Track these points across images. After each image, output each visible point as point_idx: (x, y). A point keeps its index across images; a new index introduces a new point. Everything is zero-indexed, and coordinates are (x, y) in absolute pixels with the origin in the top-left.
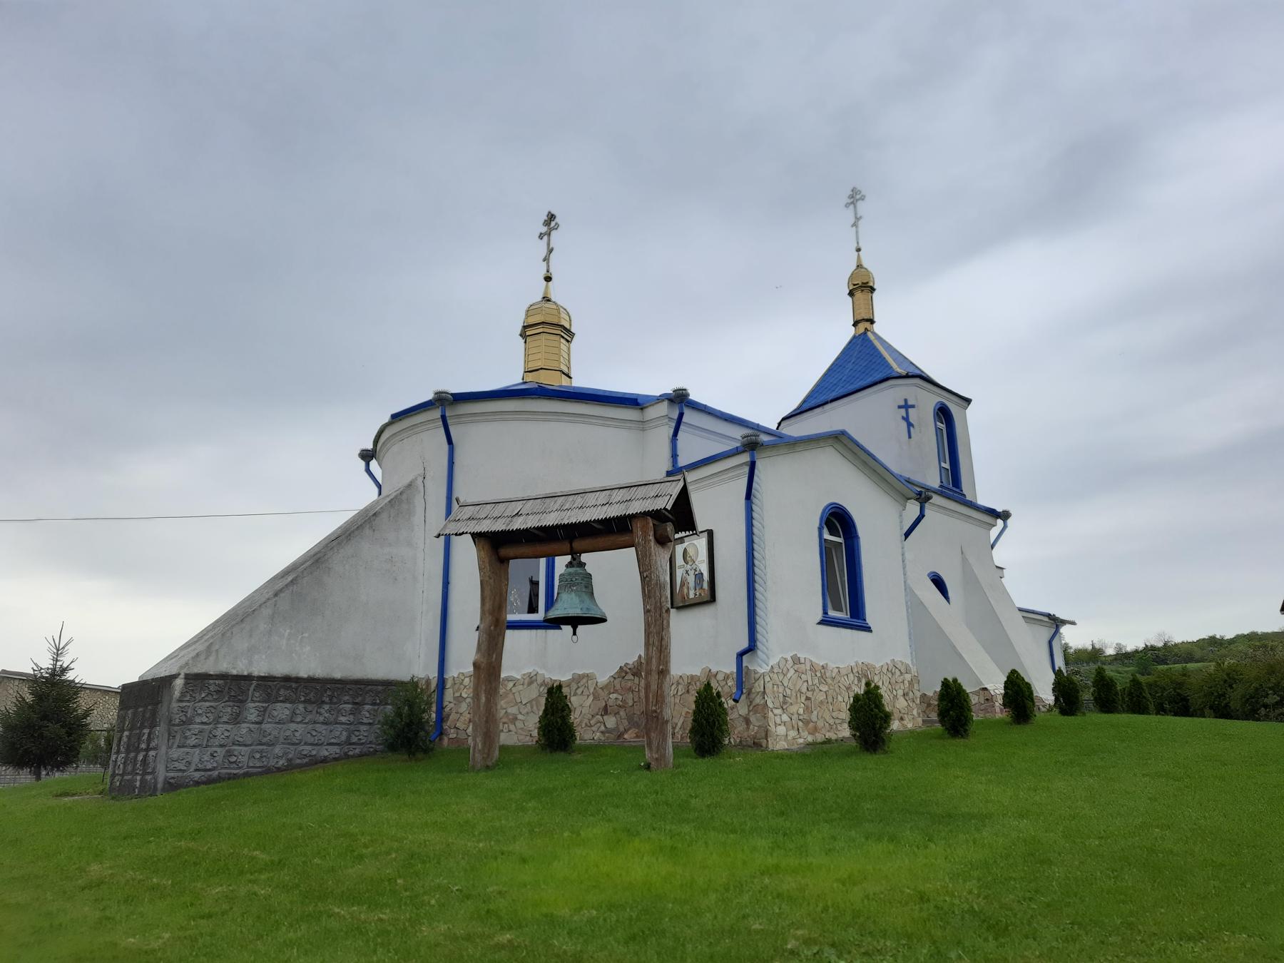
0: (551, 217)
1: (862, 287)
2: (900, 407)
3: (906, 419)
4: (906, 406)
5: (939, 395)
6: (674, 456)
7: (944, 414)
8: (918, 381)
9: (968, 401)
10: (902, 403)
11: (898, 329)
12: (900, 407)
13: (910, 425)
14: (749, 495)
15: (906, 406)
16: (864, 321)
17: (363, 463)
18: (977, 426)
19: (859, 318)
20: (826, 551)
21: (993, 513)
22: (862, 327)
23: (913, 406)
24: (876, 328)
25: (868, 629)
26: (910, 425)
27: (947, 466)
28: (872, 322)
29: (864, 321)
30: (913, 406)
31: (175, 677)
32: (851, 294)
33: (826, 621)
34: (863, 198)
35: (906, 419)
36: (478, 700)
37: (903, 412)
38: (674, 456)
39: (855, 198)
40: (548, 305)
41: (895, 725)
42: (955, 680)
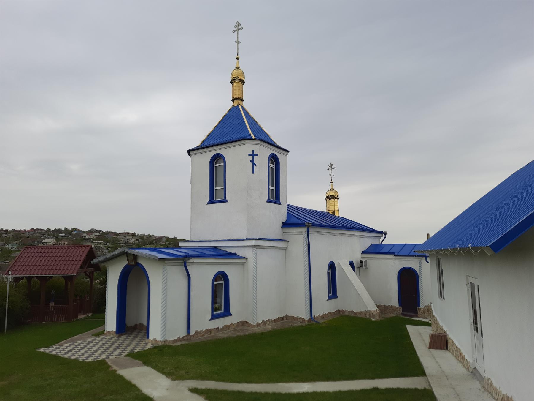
1: (237, 80)
2: (249, 155)
3: (252, 162)
4: (253, 155)
5: (273, 150)
6: (238, 33)
7: (274, 159)
8: (259, 142)
9: (288, 152)
12: (249, 155)
13: (254, 165)
14: (256, 239)
15: (253, 155)
16: (238, 99)
17: (227, 198)
18: (288, 163)
19: (235, 97)
20: (270, 169)
21: (381, 233)
22: (237, 102)
23: (257, 155)
24: (244, 104)
25: (280, 204)
26: (254, 165)
27: (274, 188)
28: (243, 100)
29: (238, 99)
30: (257, 155)
31: (422, 373)
32: (231, 82)
34: (242, 29)
35: (252, 162)
36: (178, 341)
38: (238, 33)
39: (238, 27)
41: (431, 332)
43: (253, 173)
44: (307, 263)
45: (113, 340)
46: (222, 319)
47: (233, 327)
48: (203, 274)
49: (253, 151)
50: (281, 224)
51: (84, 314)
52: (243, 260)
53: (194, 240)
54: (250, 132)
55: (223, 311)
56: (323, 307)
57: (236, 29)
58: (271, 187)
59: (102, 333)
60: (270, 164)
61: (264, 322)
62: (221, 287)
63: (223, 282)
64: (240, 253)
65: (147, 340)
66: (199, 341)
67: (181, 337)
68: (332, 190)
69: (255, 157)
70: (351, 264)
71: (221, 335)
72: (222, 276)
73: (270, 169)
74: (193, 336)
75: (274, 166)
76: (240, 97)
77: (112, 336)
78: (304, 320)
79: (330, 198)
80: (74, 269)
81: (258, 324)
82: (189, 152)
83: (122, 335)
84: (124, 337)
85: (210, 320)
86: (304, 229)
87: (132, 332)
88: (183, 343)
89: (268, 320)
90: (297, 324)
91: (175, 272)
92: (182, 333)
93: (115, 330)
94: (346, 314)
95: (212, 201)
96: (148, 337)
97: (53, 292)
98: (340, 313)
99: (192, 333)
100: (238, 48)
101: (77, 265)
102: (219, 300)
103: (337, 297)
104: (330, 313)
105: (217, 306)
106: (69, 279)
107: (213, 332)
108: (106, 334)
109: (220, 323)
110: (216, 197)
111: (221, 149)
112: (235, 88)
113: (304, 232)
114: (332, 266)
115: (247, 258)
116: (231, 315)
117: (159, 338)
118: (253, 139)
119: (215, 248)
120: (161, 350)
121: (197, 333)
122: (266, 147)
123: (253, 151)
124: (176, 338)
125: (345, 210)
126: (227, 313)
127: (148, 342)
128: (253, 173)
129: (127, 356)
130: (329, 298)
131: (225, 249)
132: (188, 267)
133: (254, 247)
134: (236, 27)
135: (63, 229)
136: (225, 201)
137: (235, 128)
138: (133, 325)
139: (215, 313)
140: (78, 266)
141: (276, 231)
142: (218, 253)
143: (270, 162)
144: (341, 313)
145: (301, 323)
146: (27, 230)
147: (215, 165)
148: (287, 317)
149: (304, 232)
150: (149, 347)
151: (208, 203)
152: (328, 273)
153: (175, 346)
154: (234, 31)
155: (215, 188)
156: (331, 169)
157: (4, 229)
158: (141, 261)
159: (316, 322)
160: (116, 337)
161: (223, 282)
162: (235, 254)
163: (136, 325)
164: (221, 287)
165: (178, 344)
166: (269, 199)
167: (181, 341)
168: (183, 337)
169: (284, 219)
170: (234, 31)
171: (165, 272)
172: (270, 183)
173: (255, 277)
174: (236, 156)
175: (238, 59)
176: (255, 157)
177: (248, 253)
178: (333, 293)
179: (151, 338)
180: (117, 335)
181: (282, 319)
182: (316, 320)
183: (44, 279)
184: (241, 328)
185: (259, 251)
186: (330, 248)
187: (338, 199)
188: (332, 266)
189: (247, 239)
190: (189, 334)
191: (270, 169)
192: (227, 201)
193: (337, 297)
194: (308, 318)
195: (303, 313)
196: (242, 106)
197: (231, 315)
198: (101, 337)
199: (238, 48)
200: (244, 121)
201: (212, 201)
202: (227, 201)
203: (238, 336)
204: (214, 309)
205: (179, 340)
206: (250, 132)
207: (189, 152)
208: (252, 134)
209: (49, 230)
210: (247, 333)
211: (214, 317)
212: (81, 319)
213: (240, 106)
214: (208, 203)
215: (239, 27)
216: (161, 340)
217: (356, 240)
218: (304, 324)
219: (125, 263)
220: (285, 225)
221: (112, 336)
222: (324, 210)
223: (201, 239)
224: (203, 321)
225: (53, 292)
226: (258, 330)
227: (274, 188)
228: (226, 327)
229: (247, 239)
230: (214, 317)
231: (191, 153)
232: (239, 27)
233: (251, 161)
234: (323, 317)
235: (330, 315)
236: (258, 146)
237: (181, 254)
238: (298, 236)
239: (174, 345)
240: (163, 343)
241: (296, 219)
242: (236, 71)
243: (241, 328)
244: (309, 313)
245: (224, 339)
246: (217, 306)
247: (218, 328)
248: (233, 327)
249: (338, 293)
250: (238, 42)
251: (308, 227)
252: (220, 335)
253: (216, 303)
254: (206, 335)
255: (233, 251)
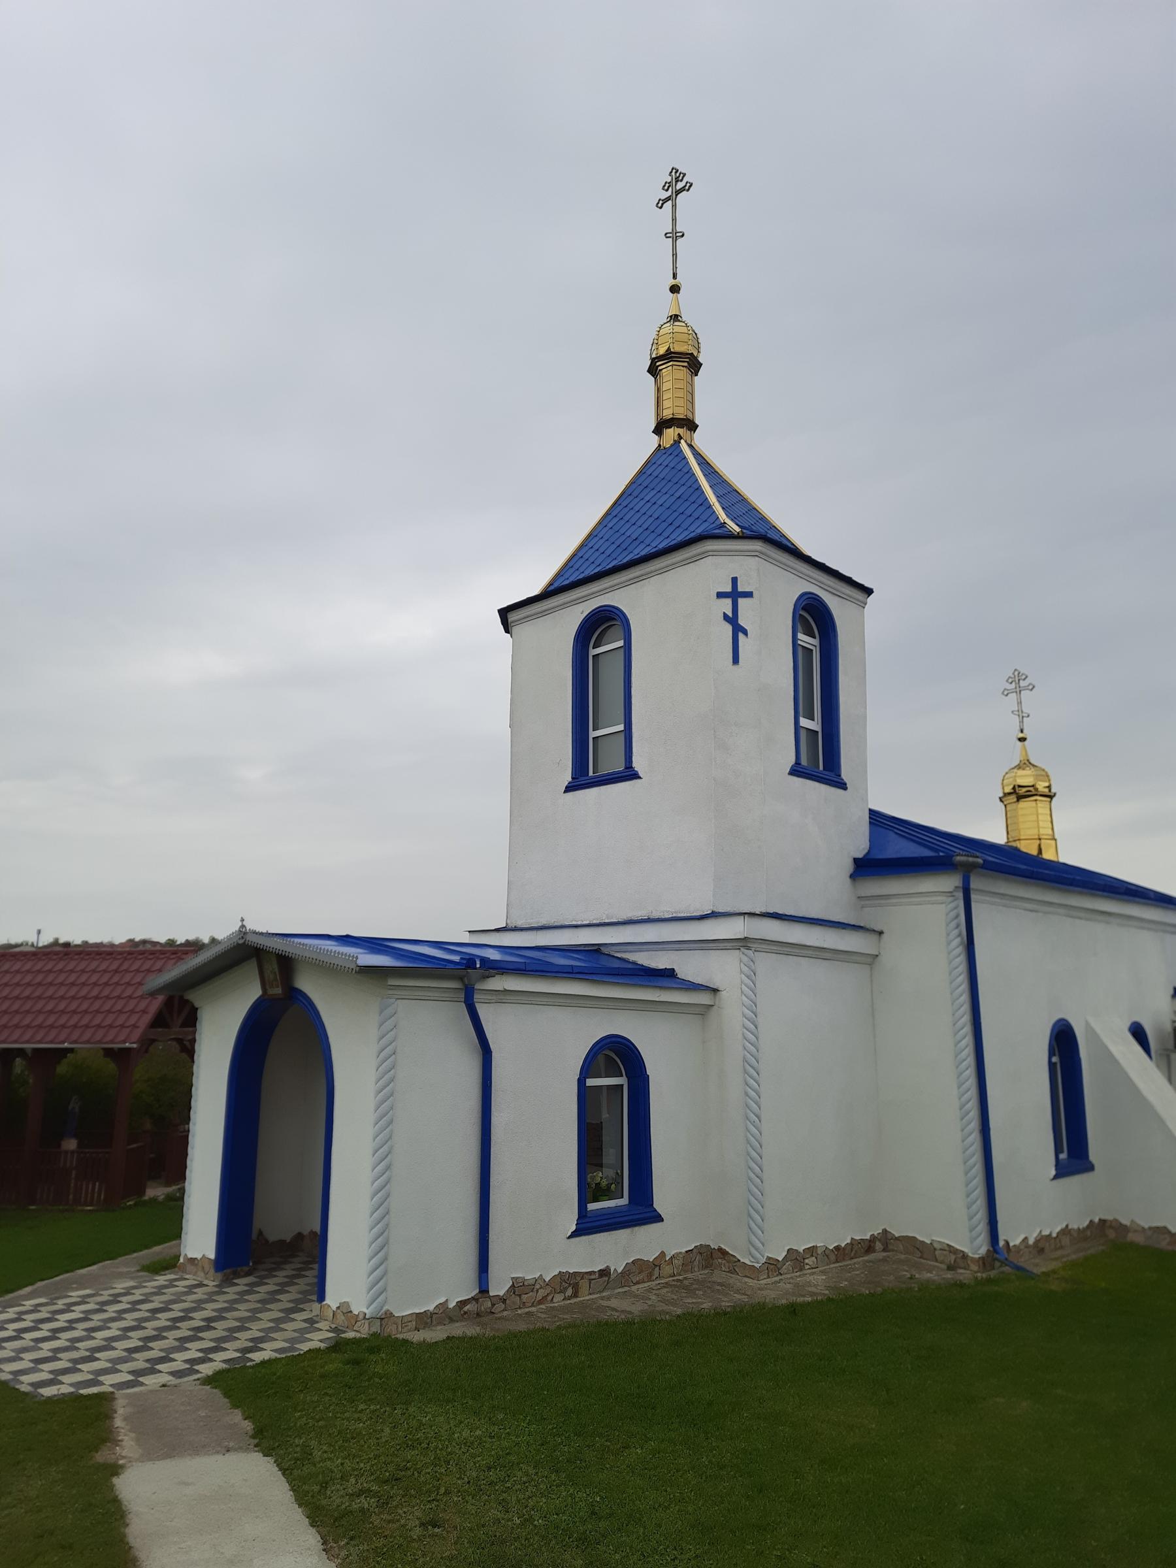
0: (677, 175)
1: (677, 359)
2: (720, 595)
3: (732, 620)
4: (735, 594)
6: (674, 206)
7: (814, 617)
8: (757, 546)
9: (869, 592)
10: (728, 588)
11: (739, 447)
12: (720, 595)
13: (738, 630)
14: (752, 914)
15: (735, 594)
16: (675, 423)
17: (637, 764)
18: (871, 639)
19: (667, 414)
22: (671, 434)
23: (749, 595)
25: (843, 786)
26: (738, 630)
27: (815, 725)
28: (692, 426)
29: (675, 423)
30: (749, 595)
32: (653, 370)
33: (797, 771)
34: (688, 187)
35: (732, 620)
37: (726, 605)
38: (674, 206)
40: (678, 327)
42: (885, 1231)
43: (736, 660)
44: (966, 1018)
45: (200, 1293)
46: (622, 1234)
47: (667, 1270)
48: (545, 1047)
49: (734, 581)
50: (849, 867)
51: (168, 1184)
52: (703, 998)
53: (520, 923)
54: (723, 516)
55: (624, 1201)
56: (1041, 1208)
57: (669, 193)
58: (804, 722)
59: (170, 1264)
60: (801, 636)
61: (796, 1258)
62: (615, 1110)
63: (621, 1080)
64: (688, 967)
65: (316, 1306)
66: (522, 1327)
67: (452, 1305)
68: (1025, 764)
69: (741, 601)
70: (1138, 1033)
71: (623, 1305)
72: (617, 1056)
73: (800, 651)
74: (503, 1300)
75: (816, 642)
76: (681, 413)
77: (201, 1276)
78: (964, 1256)
79: (1019, 794)
80: (135, 1026)
81: (772, 1265)
82: (504, 613)
83: (237, 1275)
84: (242, 1283)
85: (574, 1235)
86: (948, 882)
87: (278, 1266)
88: (458, 1329)
89: (812, 1251)
90: (934, 1275)
91: (428, 1028)
92: (453, 1285)
93: (212, 1256)
94: (1131, 1237)
95: (581, 780)
96: (321, 1297)
97: (74, 1105)
98: (1105, 1234)
99: (498, 1288)
100: (675, 255)
101: (144, 1012)
102: (609, 1156)
103: (1090, 1168)
104: (1066, 1231)
105: (599, 1177)
106: (120, 1056)
107: (584, 1284)
108: (183, 1269)
109: (614, 1250)
110: (597, 761)
111: (613, 589)
112: (665, 387)
113: (950, 894)
114: (1063, 1041)
115: (715, 991)
116: (658, 1218)
117: (359, 1307)
118: (731, 536)
119: (595, 951)
120: (356, 1362)
121: (518, 1287)
122: (786, 568)
123: (734, 581)
124: (431, 1307)
125: (1076, 835)
126: (642, 1211)
127: (321, 1317)
128: (736, 660)
129: (209, 1381)
130: (1062, 1171)
131: (632, 957)
132: (483, 1011)
133: (743, 943)
134: (667, 186)
135: (206, 940)
136: (630, 774)
137: (670, 512)
138: (288, 1237)
139: (592, 1206)
140: (147, 1019)
141: (826, 886)
142: (597, 965)
143: (799, 628)
144: (1111, 1234)
145: (950, 1268)
146: (117, 942)
147: (593, 652)
148: (886, 1239)
149: (950, 894)
150: (316, 1340)
151: (569, 789)
152: (1052, 1066)
153: (425, 1346)
154: (661, 204)
155: (593, 734)
156: (1019, 691)
157: (61, 941)
158: (306, 984)
159: (1018, 1268)
160: (211, 1284)
161: (621, 1080)
162: (670, 974)
163: (300, 1236)
164: (615, 1110)
165: (437, 1334)
166: (798, 763)
167: (452, 1320)
168: (462, 1303)
169: (860, 845)
170: (661, 204)
171: (389, 1024)
172: (802, 706)
173: (751, 1067)
174: (667, 608)
175: (675, 289)
176: (741, 601)
177: (719, 970)
178: (1073, 1150)
179: (332, 1299)
180: (219, 1275)
181: (868, 1246)
182: (1012, 1258)
183: (47, 1059)
184: (699, 1274)
185: (765, 962)
186: (1038, 966)
187: (1051, 797)
188: (1063, 1041)
189: (714, 915)
190: (484, 1290)
191: (800, 651)
192: (635, 776)
193: (1090, 1168)
194: (983, 1251)
195: (948, 1222)
196: (690, 446)
197: (658, 1218)
198: (161, 1280)
199: (675, 255)
200: (699, 488)
201: (581, 780)
202: (635, 776)
203: (687, 1315)
204: (588, 1191)
205: (442, 1315)
206: (723, 516)
207: (504, 613)
208: (728, 521)
209: (171, 943)
210: (726, 1303)
211: (587, 1225)
212: (154, 1200)
213: (683, 444)
214: (569, 789)
215: (680, 185)
216: (369, 1312)
217: (1146, 940)
218: (964, 1275)
219: (253, 993)
220: (864, 868)
221: (201, 1276)
222: (998, 836)
223: (543, 921)
224: (543, 1240)
225: (74, 1105)
226: (774, 1292)
227: (815, 725)
228: (640, 1269)
229: (714, 915)
230: (587, 1225)
231: (512, 617)
232: (680, 185)
233: (726, 617)
234: (1041, 1246)
235: (1066, 1241)
236: (753, 562)
237: (456, 958)
238: (922, 910)
239: (417, 1337)
240: (376, 1328)
241: (900, 852)
242: (667, 329)
243: (699, 1274)
244: (982, 1228)
245: (629, 1323)
246: (599, 1177)
247: (605, 1273)
248: (667, 1270)
249: (1095, 1152)
250: (675, 236)
251: (967, 871)
252: (614, 1303)
253: (600, 1166)
254: (558, 1298)
255: (659, 961)
